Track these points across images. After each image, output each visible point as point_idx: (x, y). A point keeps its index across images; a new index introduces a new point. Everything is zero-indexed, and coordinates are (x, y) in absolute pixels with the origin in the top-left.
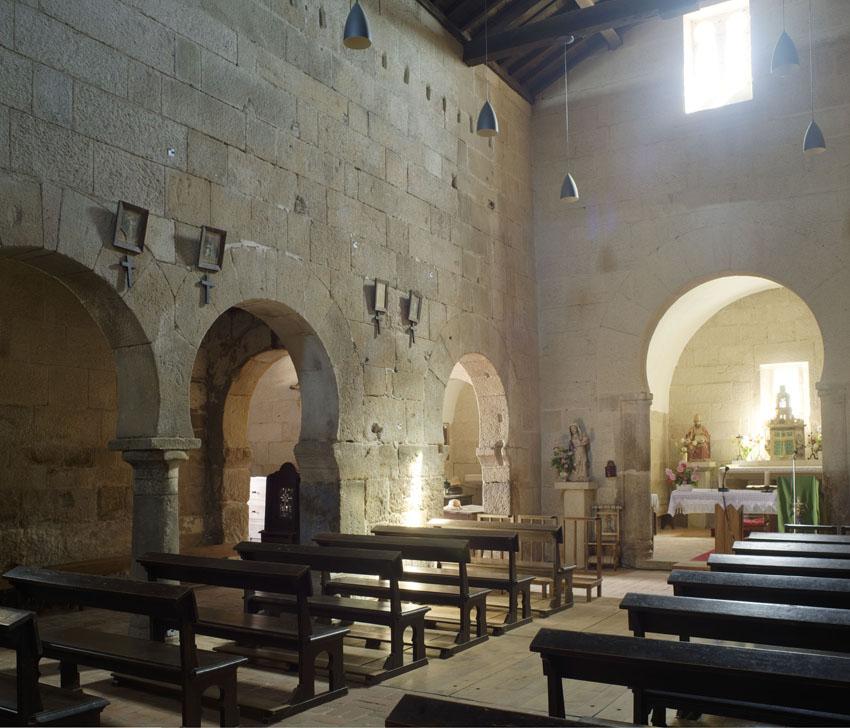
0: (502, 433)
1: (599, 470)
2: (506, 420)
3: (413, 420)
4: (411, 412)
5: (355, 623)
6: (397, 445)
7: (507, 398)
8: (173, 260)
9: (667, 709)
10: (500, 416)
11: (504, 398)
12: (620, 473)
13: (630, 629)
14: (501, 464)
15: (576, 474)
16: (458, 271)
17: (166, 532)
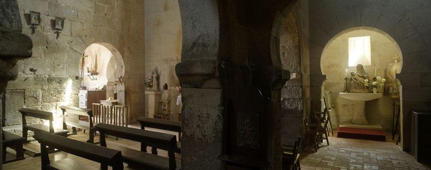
1: (162, 87)
2: (124, 68)
4: (56, 64)
5: (323, 74)
7: (124, 60)
9: (370, 37)
11: (122, 59)
12: (169, 88)
15: (153, 88)
16: (92, 10)
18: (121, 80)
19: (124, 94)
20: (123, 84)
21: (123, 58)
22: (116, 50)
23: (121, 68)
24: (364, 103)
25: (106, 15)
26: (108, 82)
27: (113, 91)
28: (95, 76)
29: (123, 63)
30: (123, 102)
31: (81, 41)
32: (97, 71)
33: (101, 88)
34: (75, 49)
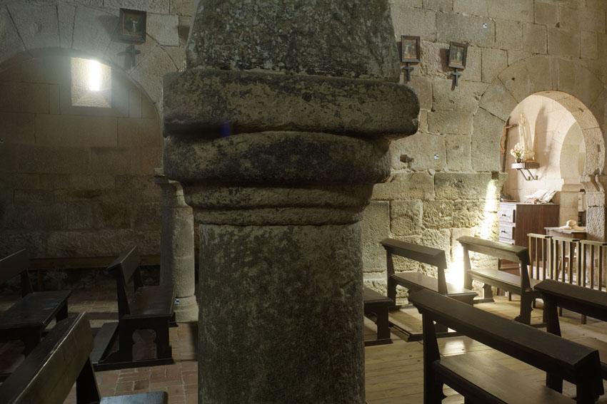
0: (600, 162)
2: (603, 150)
3: (455, 151)
4: (452, 145)
6: (433, 173)
8: (178, 43)
10: (598, 146)
11: (599, 130)
13: (513, 239)
14: (599, 190)
16: (526, 19)
17: (173, 234)
22: (583, 106)
23: (596, 150)
25: (558, 25)
26: (565, 186)
27: (575, 206)
28: (533, 171)
31: (503, 92)
32: (539, 161)
33: (547, 198)
34: (490, 109)
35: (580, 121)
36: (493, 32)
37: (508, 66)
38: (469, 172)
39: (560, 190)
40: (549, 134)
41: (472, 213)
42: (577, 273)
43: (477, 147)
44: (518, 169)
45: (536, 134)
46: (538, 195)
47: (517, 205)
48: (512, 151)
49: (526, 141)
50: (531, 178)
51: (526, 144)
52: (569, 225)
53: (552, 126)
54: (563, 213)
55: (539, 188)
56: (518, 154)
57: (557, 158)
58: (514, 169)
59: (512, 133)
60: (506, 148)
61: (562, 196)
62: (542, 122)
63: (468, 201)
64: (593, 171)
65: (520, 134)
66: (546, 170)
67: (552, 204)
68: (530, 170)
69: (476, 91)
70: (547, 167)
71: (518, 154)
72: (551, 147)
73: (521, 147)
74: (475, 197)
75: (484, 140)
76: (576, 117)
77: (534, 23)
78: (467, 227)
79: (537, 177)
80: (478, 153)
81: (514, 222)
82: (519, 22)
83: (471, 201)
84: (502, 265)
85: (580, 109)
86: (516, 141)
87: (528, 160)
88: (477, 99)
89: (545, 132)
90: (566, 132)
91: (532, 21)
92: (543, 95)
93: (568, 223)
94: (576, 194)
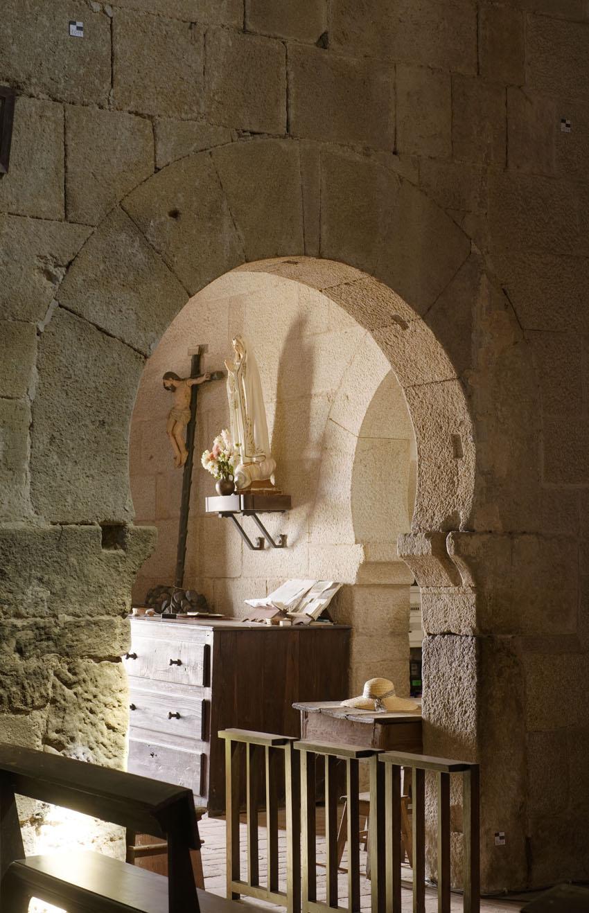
0: (460, 491)
10: (456, 441)
11: (455, 387)
14: (456, 581)
18: (449, 542)
19: (470, 657)
20: (466, 578)
21: (462, 379)
22: (407, 312)
23: (447, 453)
24: (292, 505)
25: (323, 42)
26: (366, 566)
27: (401, 628)
28: (272, 522)
29: (463, 415)
30: (465, 722)
31: (141, 257)
32: (290, 489)
33: (314, 606)
34: (97, 313)
35: (400, 364)
36: (106, 50)
37: (157, 170)
38: (21, 525)
39: (351, 579)
40: (318, 405)
41: (33, 663)
42: (467, 829)
43: (53, 438)
44: (227, 514)
45: (280, 402)
46: (284, 596)
47: (217, 631)
48: (206, 455)
49: (248, 425)
50: (266, 543)
51: (249, 435)
52: (372, 696)
53: (326, 378)
54: (363, 651)
55: (288, 574)
56: (224, 467)
57: (341, 483)
58: (213, 515)
59: (208, 399)
60: (190, 446)
61: (358, 597)
62: (298, 363)
63: (19, 623)
64: (439, 519)
65: (230, 401)
66: (310, 516)
67: (327, 623)
68: (263, 517)
69: (45, 253)
70: (313, 507)
71: (224, 467)
72: (324, 445)
73: (232, 444)
74: (45, 609)
75: (75, 417)
76: (385, 345)
77: (245, 31)
78: (17, 711)
79: (284, 537)
80: (54, 458)
81: (206, 684)
82: (193, 24)
83: (31, 620)
84: (138, 838)
85: (396, 319)
86: (223, 424)
87: (253, 484)
88: (51, 277)
89: (307, 396)
90: (368, 396)
91: (237, 22)
92: (277, 271)
93: (366, 688)
94: (401, 592)
